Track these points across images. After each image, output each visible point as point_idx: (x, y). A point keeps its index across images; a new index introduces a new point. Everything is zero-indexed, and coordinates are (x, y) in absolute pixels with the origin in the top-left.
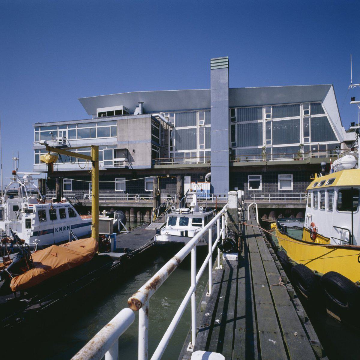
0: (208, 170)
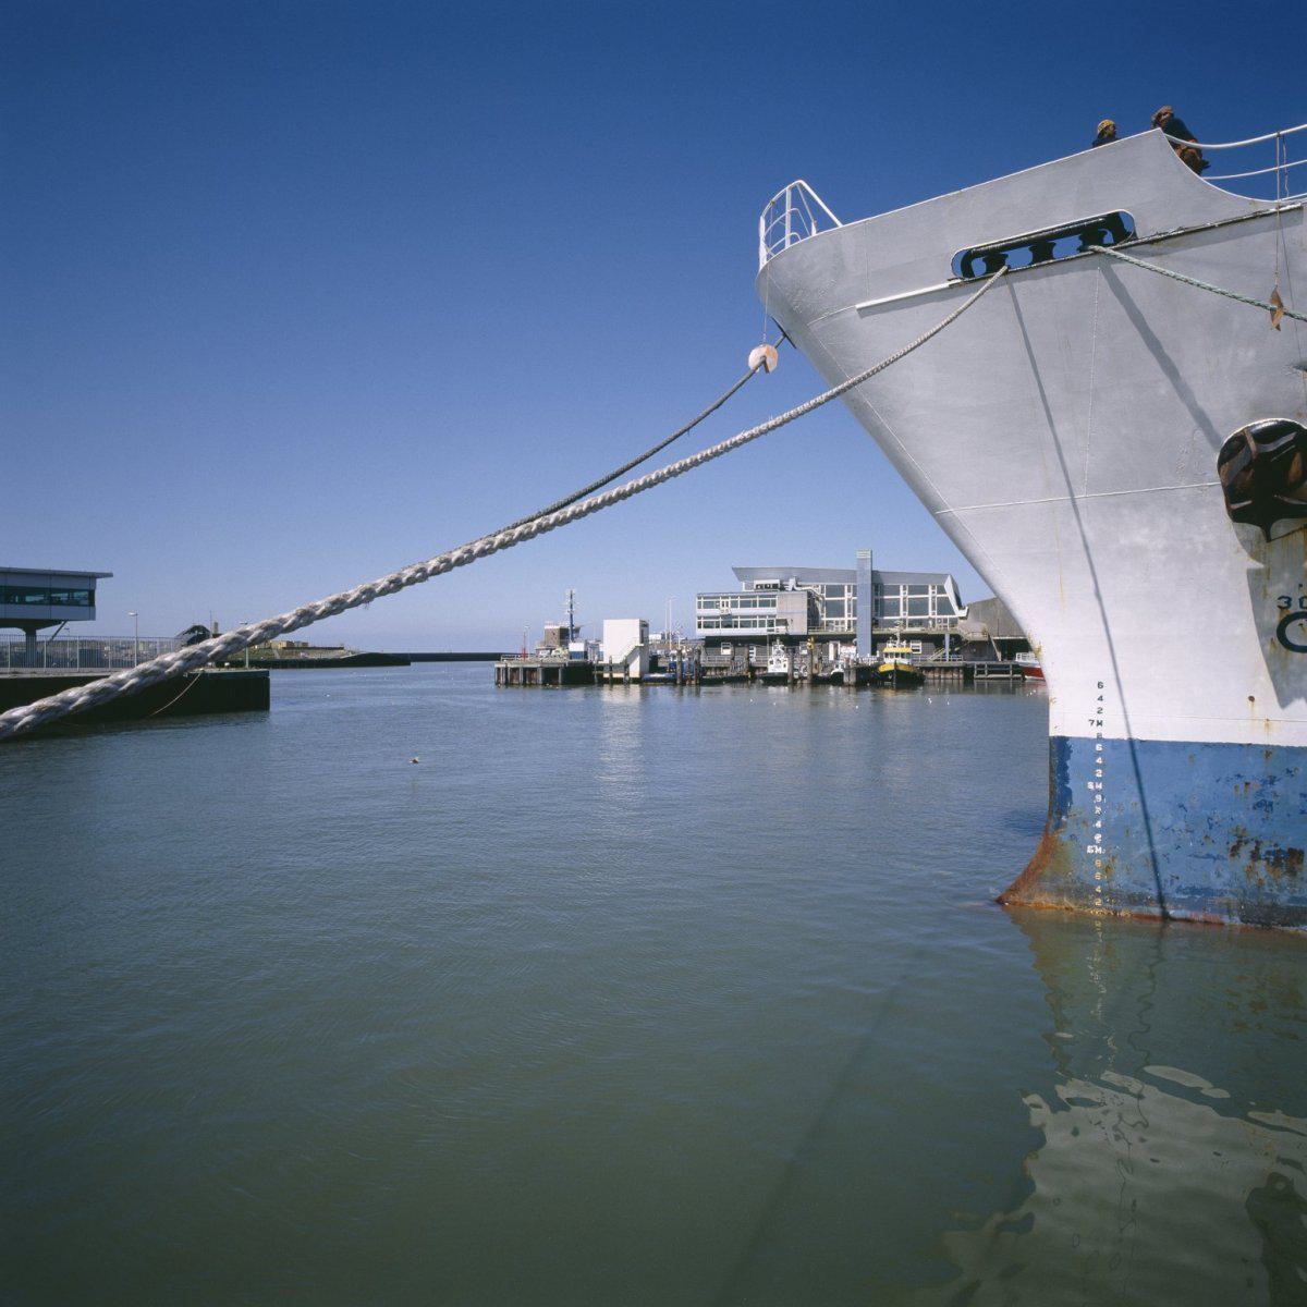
0: (854, 636)
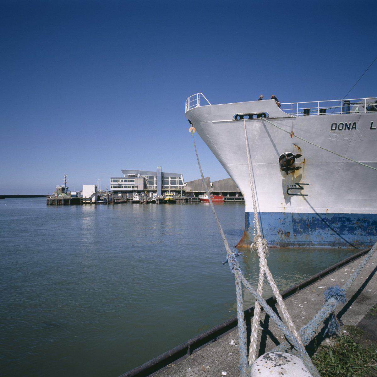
0: (157, 191)
